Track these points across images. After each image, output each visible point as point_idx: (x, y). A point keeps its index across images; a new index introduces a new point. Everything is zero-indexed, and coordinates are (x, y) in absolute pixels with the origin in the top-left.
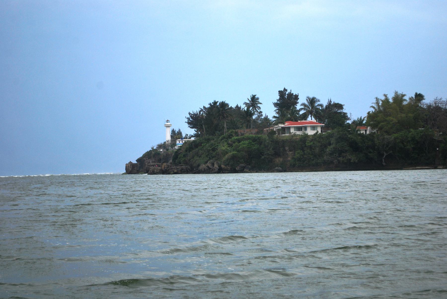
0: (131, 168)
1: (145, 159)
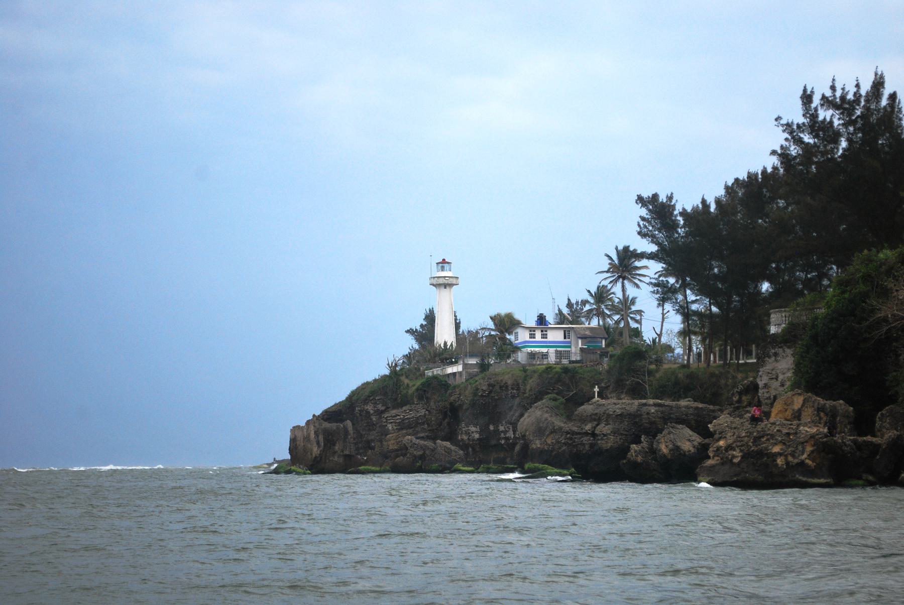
0: (318, 443)
1: (370, 408)
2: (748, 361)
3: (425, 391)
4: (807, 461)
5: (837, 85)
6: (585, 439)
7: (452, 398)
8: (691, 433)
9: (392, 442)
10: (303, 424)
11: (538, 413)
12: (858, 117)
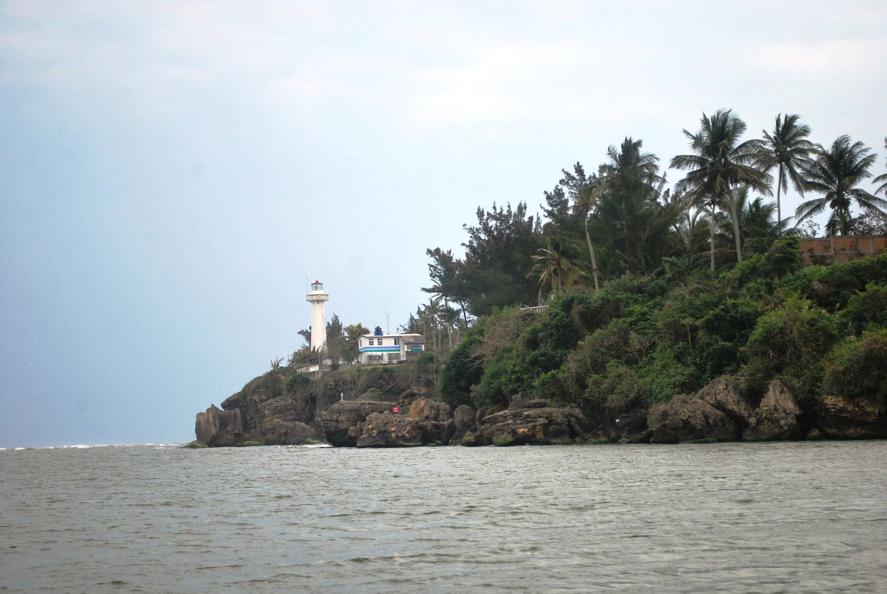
0: (215, 425)
1: (256, 398)
3: (292, 385)
5: (496, 206)
7: (311, 391)
10: (204, 411)
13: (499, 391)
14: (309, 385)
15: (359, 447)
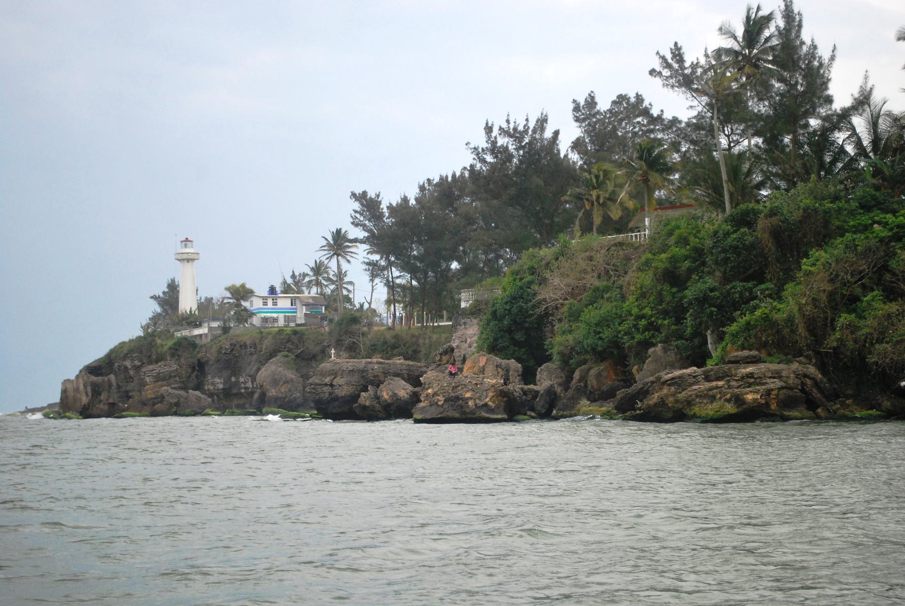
0: (86, 393)
1: (128, 363)
2: (440, 324)
3: (176, 350)
4: (489, 403)
6: (325, 389)
7: (200, 355)
8: (404, 383)
9: (150, 391)
11: (274, 367)
12: (527, 143)
13: (616, 344)
14: (198, 350)
15: (417, 421)
